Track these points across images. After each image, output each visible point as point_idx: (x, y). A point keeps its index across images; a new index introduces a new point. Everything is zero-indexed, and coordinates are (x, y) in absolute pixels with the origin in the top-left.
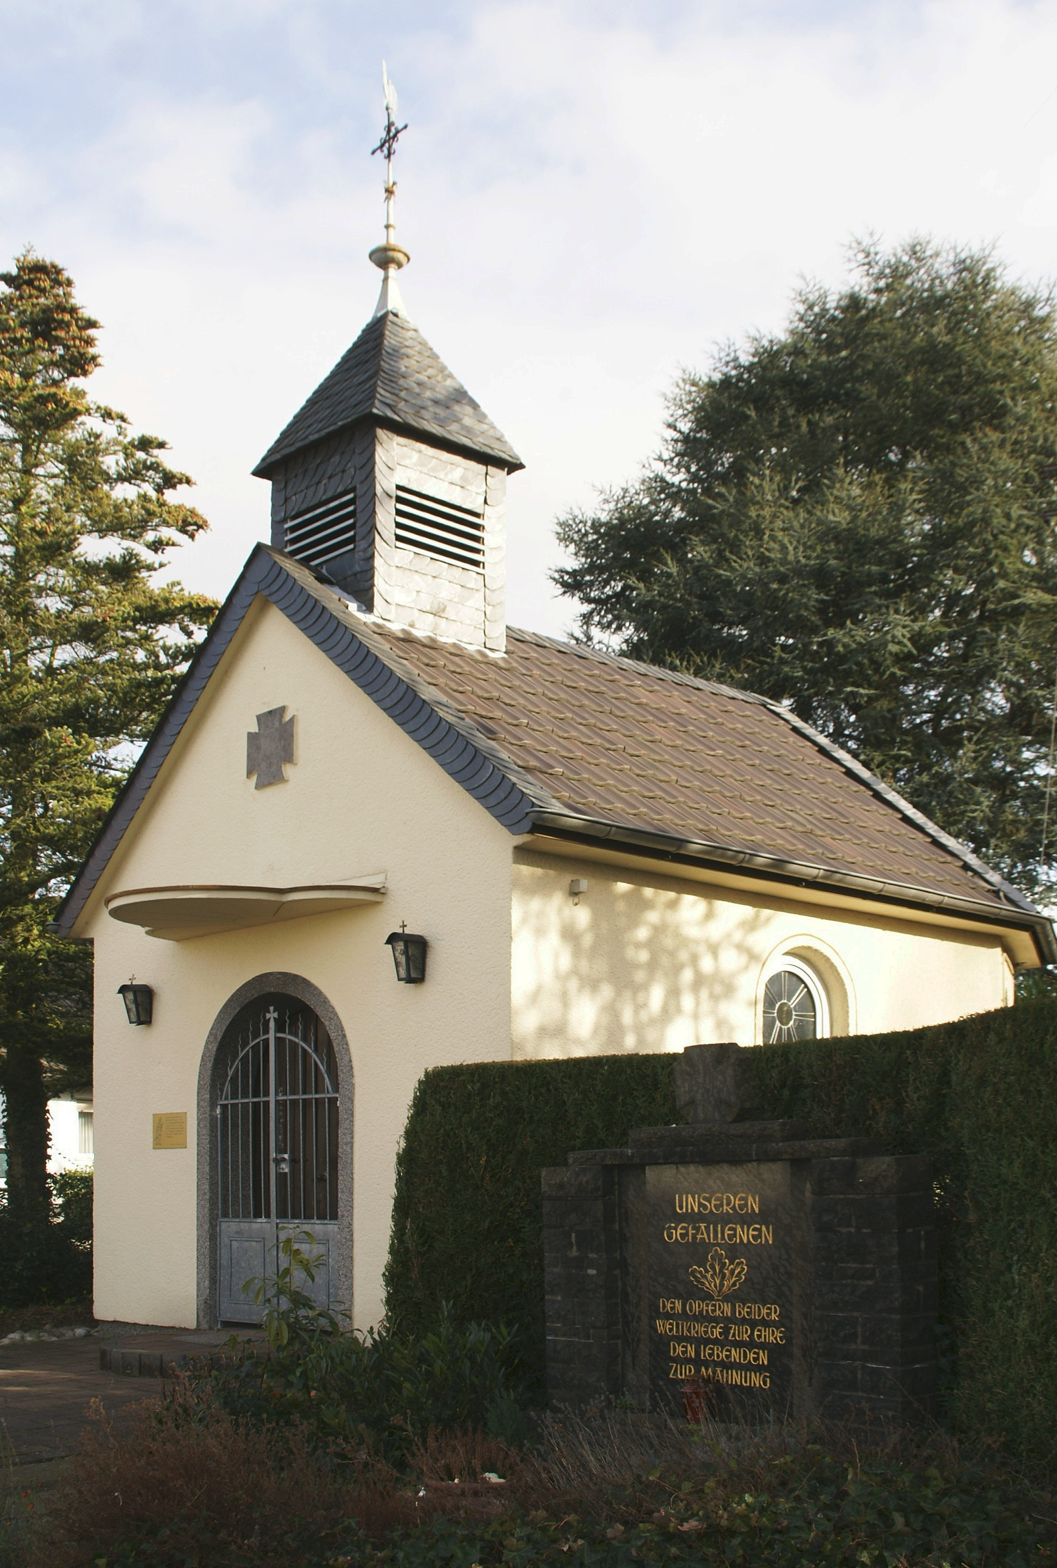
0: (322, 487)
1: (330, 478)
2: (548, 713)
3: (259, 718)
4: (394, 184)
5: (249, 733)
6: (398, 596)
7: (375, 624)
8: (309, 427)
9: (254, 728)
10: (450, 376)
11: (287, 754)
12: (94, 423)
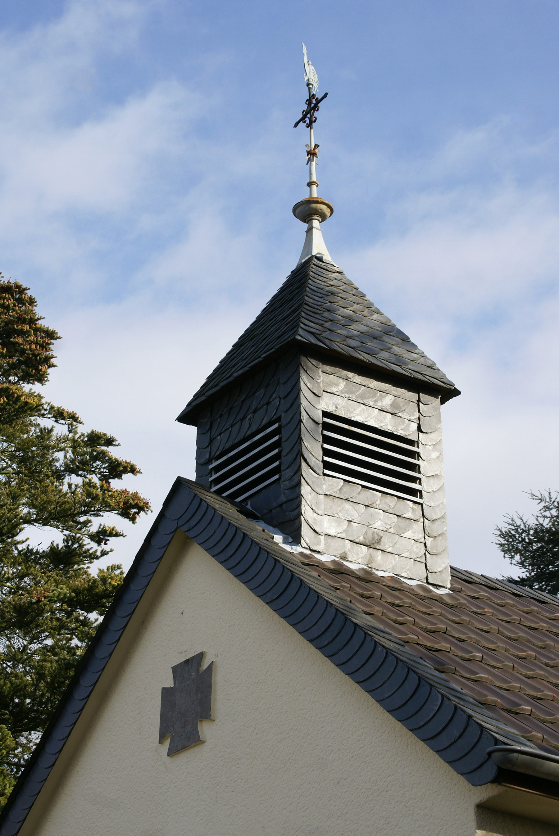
0: (246, 422)
1: (254, 412)
2: (506, 650)
3: (175, 670)
4: (317, 146)
5: (164, 689)
6: (327, 526)
7: (301, 554)
8: (234, 366)
9: (169, 683)
10: (377, 312)
11: (204, 710)
12: (46, 423)
